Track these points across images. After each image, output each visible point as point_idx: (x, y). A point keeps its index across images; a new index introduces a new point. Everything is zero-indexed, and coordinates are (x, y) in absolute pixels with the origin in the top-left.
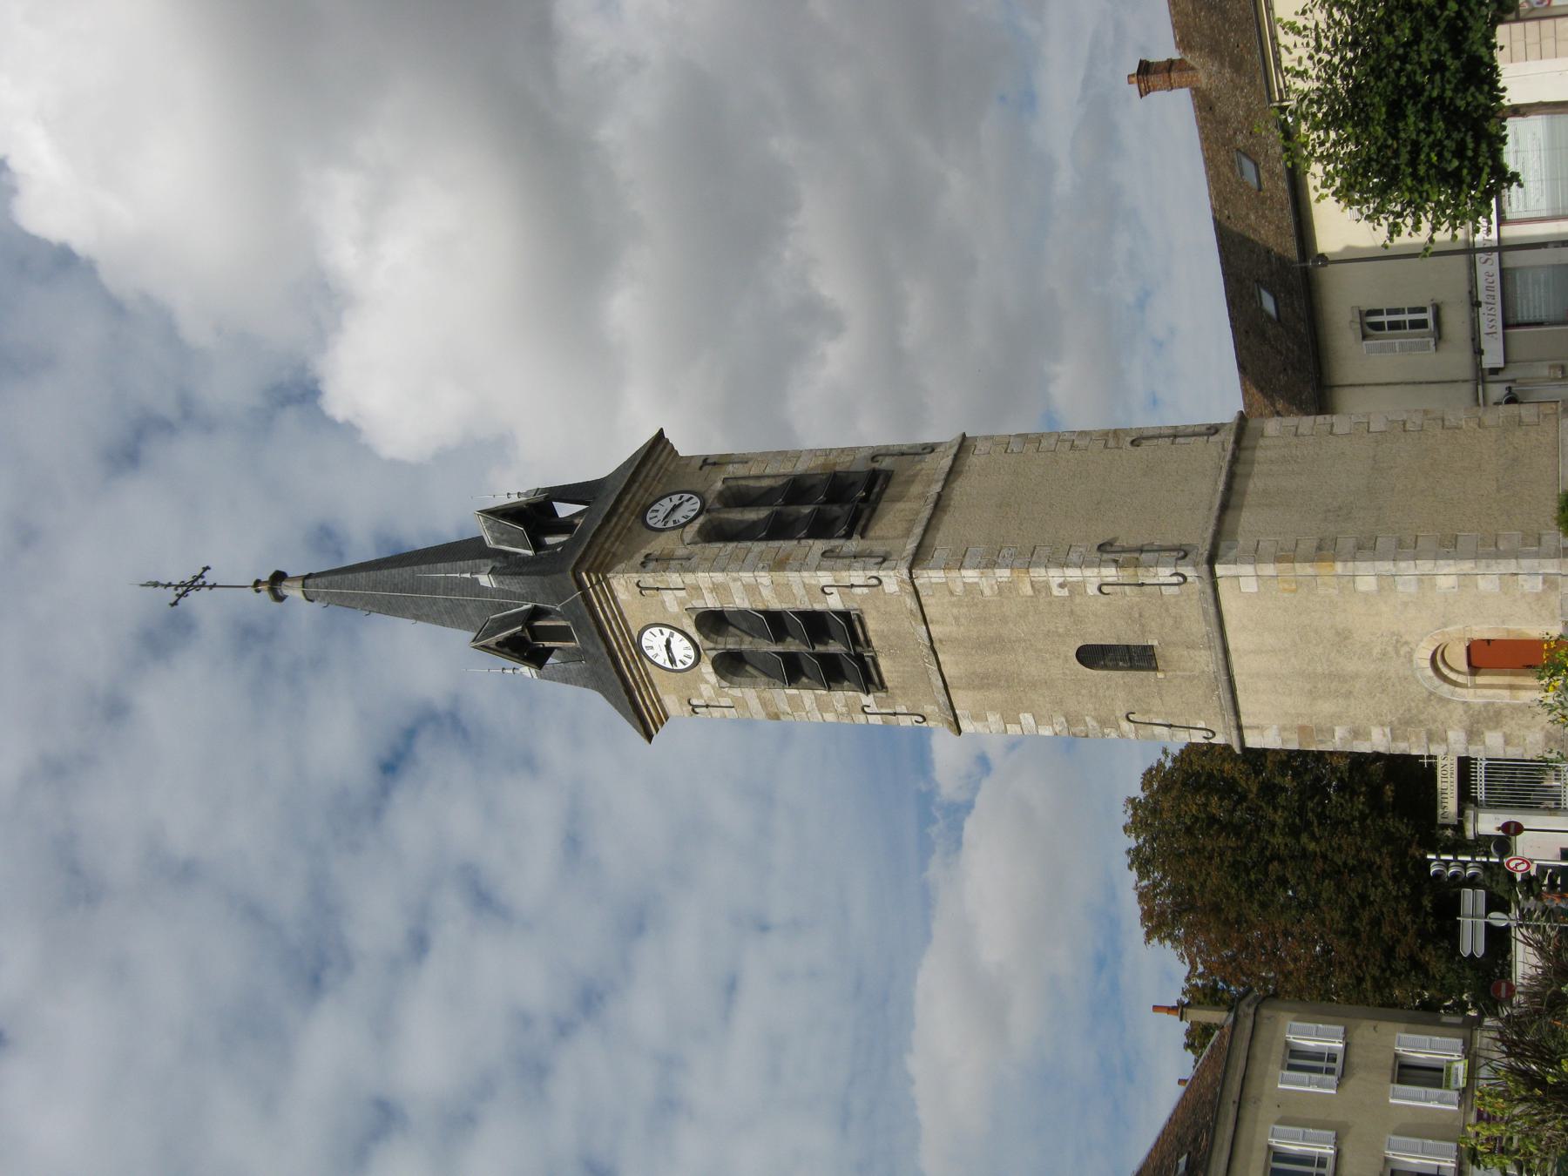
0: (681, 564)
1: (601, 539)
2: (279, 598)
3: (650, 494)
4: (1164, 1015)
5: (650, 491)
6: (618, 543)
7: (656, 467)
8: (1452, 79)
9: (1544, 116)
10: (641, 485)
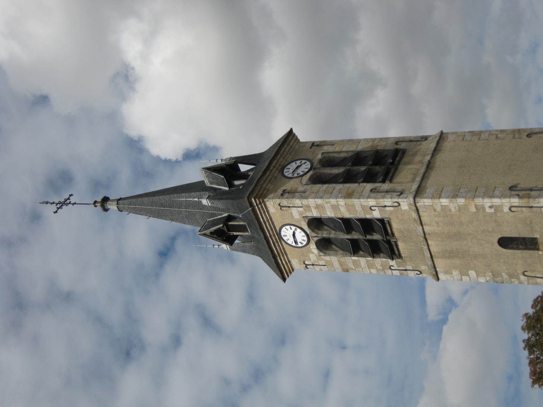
0: (301, 195)
7: (289, 147)
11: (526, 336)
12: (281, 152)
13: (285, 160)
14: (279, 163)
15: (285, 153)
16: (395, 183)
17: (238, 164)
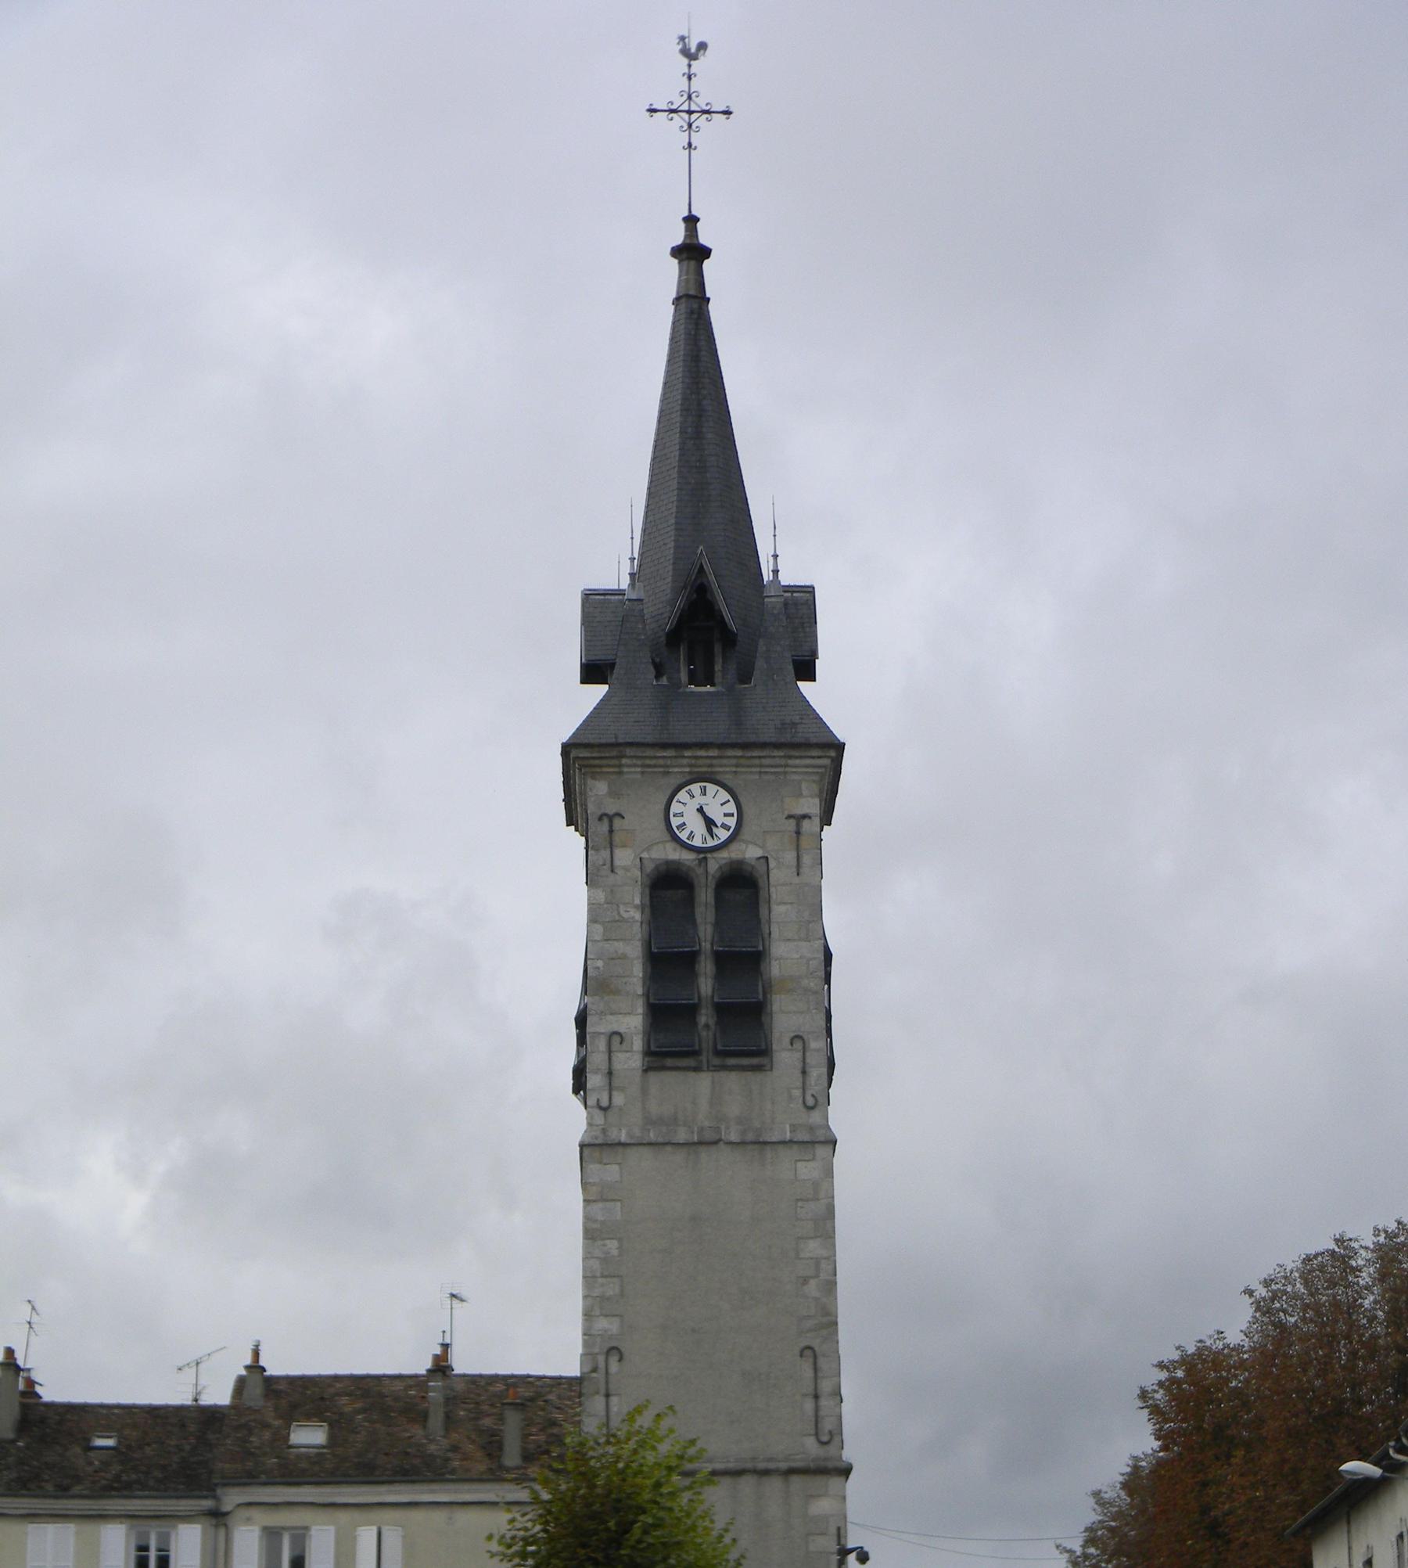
0: (604, 865)
1: (629, 751)
2: (702, 46)
3: (760, 772)
4: (41, 1382)
5: (739, 769)
6: (639, 769)
7: (783, 762)
8: (620, 947)
9: (1314, 1554)
10: (741, 757)
11: (1166, 1361)
12: (756, 753)
13: (734, 769)
14: (715, 762)
15: (757, 762)
16: (644, 1091)
17: (605, 688)
